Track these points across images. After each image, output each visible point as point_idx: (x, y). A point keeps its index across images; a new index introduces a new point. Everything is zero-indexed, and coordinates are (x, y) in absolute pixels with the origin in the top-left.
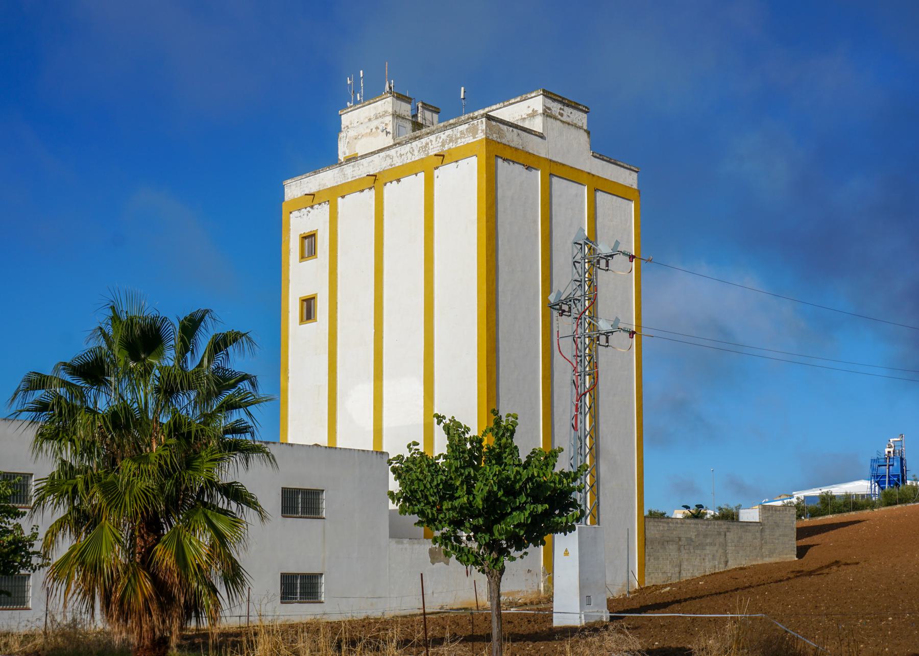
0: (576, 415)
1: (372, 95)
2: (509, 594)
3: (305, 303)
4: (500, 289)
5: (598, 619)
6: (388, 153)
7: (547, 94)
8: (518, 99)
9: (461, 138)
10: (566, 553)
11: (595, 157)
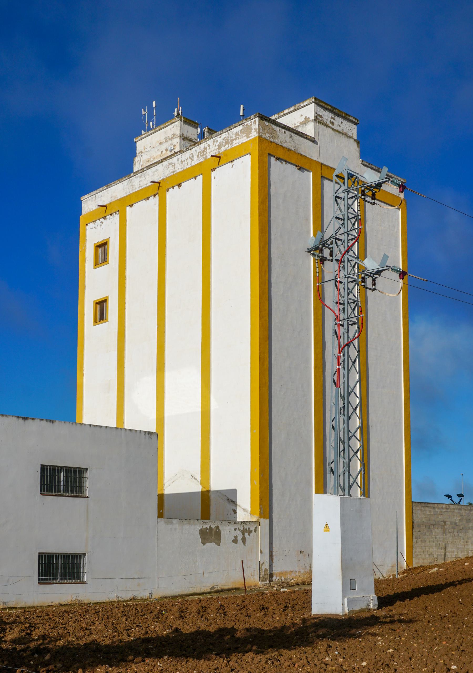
0: (338, 369)
1: (163, 120)
2: (281, 574)
3: (98, 306)
4: (273, 280)
5: (363, 606)
6: (170, 161)
7: (318, 102)
8: (292, 109)
9: (236, 139)
10: (327, 528)
11: (365, 165)
